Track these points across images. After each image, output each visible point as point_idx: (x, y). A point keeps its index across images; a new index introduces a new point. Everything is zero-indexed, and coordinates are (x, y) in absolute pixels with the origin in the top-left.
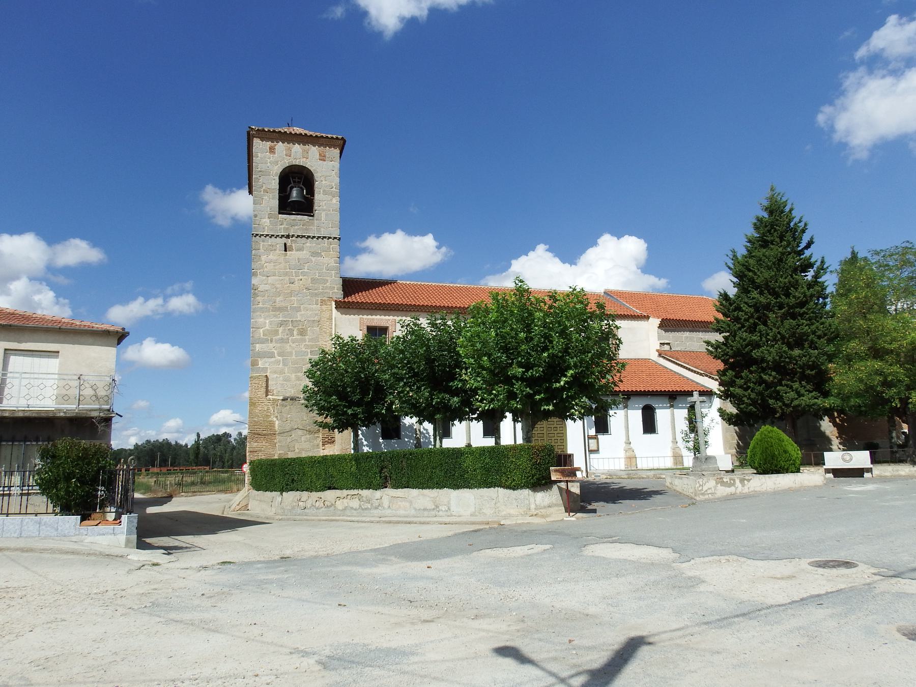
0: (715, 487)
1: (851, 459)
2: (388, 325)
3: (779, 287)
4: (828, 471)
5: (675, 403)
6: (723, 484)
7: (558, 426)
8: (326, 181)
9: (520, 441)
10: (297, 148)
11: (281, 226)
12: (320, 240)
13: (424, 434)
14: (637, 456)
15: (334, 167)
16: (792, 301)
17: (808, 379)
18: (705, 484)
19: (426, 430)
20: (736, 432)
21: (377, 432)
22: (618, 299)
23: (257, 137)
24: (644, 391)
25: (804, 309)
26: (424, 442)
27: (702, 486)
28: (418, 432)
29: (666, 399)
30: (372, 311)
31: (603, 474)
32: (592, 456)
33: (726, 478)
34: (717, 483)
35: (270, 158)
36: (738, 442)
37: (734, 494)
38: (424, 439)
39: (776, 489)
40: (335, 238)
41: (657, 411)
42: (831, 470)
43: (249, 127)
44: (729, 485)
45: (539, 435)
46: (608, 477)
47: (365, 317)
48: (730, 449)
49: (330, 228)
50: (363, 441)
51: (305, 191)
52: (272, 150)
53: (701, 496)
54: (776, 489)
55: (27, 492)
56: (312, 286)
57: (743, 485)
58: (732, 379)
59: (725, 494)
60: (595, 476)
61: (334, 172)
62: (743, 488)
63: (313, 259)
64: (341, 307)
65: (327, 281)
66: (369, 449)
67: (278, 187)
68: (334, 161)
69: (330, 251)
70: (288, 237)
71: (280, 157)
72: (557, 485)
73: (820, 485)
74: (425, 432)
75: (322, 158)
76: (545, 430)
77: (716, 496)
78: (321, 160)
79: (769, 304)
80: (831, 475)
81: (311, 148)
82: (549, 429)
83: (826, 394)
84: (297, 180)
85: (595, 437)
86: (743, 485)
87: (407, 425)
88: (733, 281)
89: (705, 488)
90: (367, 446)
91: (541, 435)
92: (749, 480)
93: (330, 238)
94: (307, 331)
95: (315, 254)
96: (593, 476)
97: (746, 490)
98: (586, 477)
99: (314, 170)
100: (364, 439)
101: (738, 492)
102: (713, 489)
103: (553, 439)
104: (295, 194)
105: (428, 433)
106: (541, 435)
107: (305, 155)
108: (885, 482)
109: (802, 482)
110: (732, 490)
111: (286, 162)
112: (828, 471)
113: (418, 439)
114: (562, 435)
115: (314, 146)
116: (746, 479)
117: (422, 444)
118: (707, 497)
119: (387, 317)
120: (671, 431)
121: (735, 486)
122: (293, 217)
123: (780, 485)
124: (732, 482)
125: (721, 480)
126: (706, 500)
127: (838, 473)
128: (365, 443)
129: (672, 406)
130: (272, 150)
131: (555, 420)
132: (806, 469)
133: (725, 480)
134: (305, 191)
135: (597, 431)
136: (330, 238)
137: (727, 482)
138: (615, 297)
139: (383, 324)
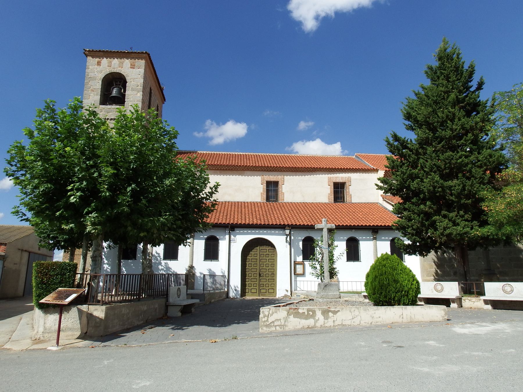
0: (286, 319)
1: (512, 291)
3: (438, 122)
4: (486, 302)
5: (378, 236)
6: (298, 315)
7: (270, 253)
8: (134, 82)
10: (116, 62)
13: (156, 257)
14: (340, 280)
15: (140, 72)
16: (448, 133)
17: (465, 208)
18: (272, 315)
19: (159, 254)
20: (434, 262)
22: (362, 159)
23: (89, 56)
24: (369, 225)
25: (462, 141)
26: (155, 263)
27: (268, 316)
28: (150, 255)
29: (370, 233)
31: (302, 294)
32: (299, 279)
33: (303, 309)
34: (289, 314)
35: (97, 69)
36: (436, 270)
37: (312, 327)
38: (155, 260)
39: (373, 323)
41: (361, 242)
42: (489, 302)
43: (84, 49)
44: (307, 317)
45: (270, 261)
46: (306, 297)
48: (428, 276)
51: (122, 90)
52: (99, 64)
53: (265, 328)
54: (373, 323)
57: (326, 318)
58: (398, 211)
59: (299, 327)
60: (297, 296)
61: (140, 76)
62: (326, 321)
66: (109, 266)
67: (100, 87)
68: (141, 69)
71: (104, 67)
72: (77, 307)
73: (438, 320)
74: (157, 255)
75: (132, 67)
76: (258, 256)
77: (287, 329)
78: (132, 68)
79: (427, 138)
80: (489, 307)
81: (125, 61)
82: (262, 256)
83: (484, 223)
84: (118, 83)
85: (302, 264)
86: (326, 318)
88: (406, 124)
89: (271, 319)
90: (107, 264)
91: (255, 260)
92: (335, 313)
96: (295, 296)
97: (330, 323)
98: (290, 296)
99: (126, 75)
100: (105, 259)
101: (318, 324)
102: (283, 322)
103: (265, 263)
104: (115, 92)
105: (160, 256)
106: (255, 260)
107: (121, 65)
108: (430, 322)
109: (413, 316)
110: (310, 322)
111: (108, 71)
112: (486, 302)
115: (128, 59)
116: (331, 311)
117: (153, 264)
118: (273, 329)
121: (314, 319)
122: (109, 107)
123: (380, 319)
124: (311, 313)
125: (296, 311)
126: (271, 333)
127: (497, 305)
128: (106, 262)
129: (375, 239)
130: (99, 64)
131: (268, 248)
132: (468, 299)
133: (301, 311)
134: (122, 90)
135: (304, 258)
137: (304, 313)
138: (361, 158)
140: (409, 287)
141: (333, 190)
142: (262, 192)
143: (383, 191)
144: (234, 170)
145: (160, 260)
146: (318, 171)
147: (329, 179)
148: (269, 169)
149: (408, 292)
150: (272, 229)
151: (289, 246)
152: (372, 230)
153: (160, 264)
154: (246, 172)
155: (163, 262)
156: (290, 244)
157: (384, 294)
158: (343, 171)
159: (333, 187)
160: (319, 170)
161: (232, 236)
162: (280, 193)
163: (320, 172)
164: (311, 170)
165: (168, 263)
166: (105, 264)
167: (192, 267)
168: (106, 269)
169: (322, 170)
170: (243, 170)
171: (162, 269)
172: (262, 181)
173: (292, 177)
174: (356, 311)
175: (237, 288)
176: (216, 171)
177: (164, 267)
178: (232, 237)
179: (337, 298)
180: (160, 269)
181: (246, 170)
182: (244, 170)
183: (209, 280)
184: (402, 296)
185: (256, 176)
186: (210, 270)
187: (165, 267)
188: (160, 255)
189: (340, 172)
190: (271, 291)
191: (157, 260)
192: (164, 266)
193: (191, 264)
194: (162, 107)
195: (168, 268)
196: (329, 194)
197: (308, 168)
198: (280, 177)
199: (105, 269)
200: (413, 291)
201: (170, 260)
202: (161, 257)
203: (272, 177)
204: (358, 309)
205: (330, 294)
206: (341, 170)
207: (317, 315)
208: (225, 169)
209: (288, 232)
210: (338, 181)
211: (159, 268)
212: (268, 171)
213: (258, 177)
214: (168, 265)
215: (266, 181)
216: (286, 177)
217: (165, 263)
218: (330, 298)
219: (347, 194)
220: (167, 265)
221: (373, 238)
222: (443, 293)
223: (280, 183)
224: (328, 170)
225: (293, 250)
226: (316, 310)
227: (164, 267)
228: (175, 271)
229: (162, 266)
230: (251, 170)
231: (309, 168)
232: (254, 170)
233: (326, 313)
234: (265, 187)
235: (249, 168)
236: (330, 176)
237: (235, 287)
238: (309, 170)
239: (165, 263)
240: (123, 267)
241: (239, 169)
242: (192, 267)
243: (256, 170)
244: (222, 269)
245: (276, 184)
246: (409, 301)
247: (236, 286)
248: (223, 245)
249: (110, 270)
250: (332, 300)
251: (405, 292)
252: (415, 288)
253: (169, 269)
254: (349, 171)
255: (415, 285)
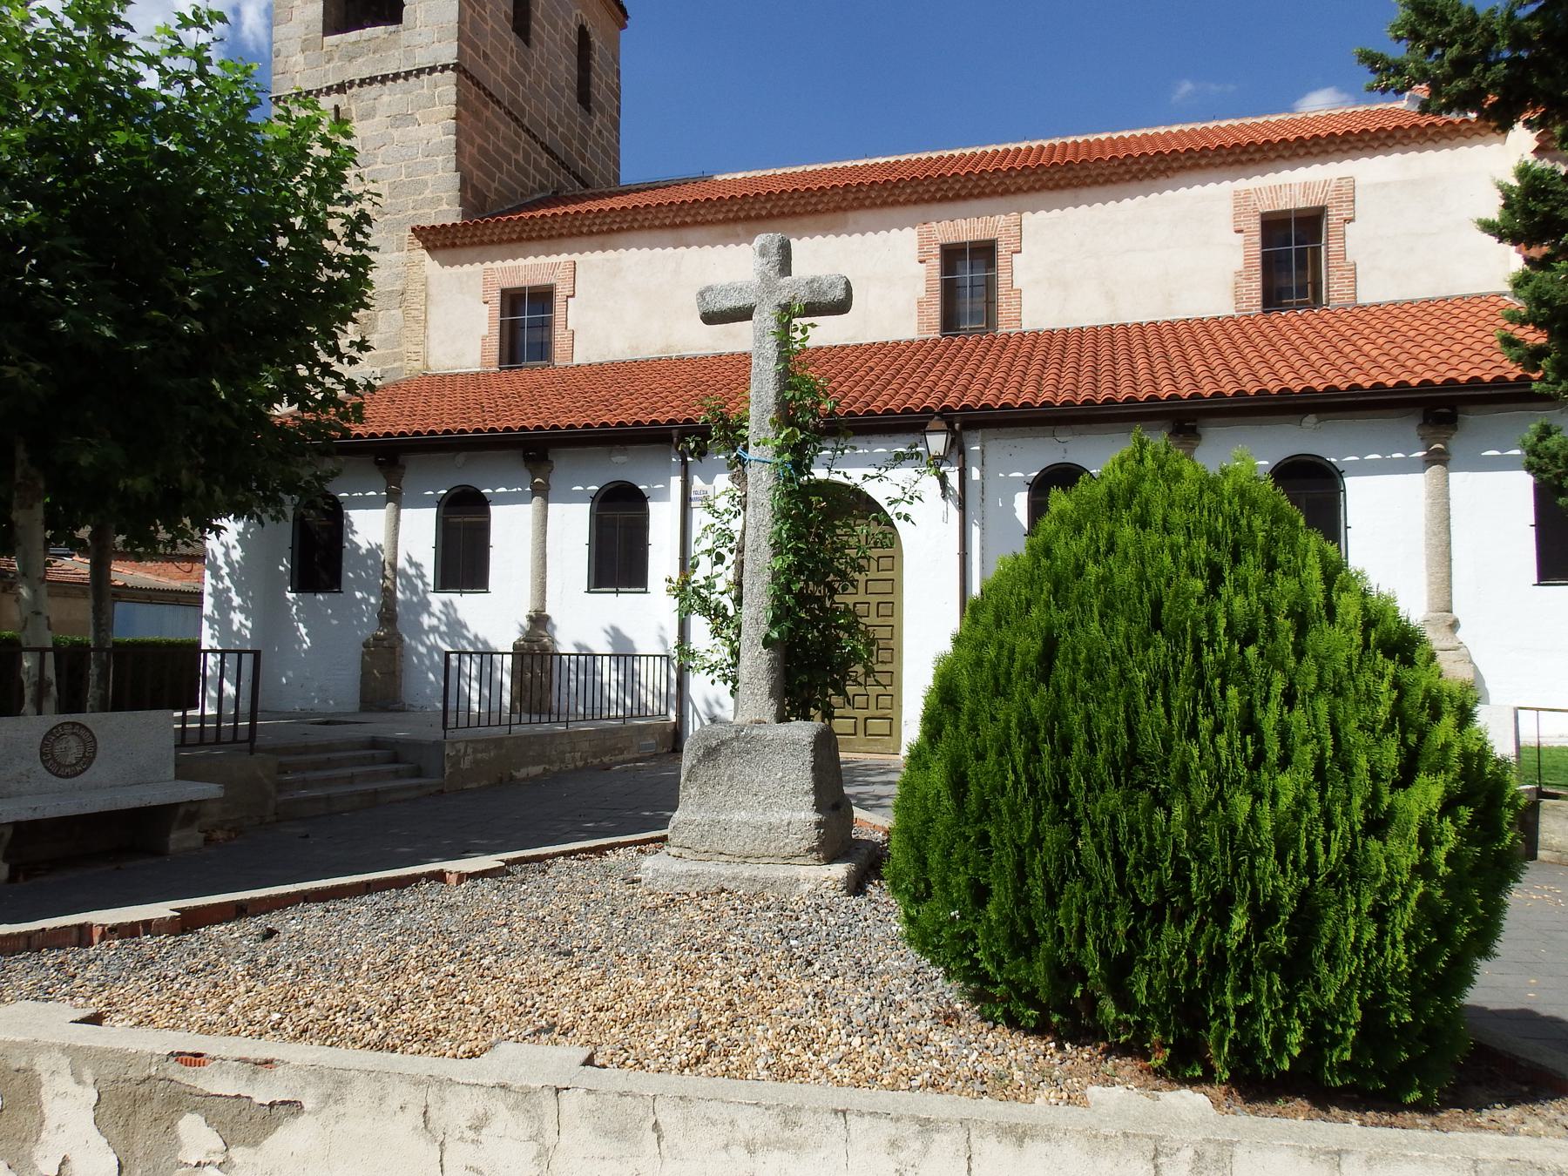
2: (553, 281)
5: (1457, 444)
9: (88, 561)
11: (327, 66)
12: (412, 80)
13: (408, 578)
19: (417, 566)
21: (281, 568)
26: (408, 604)
28: (388, 572)
29: (1410, 425)
30: (513, 246)
40: (445, 67)
41: (1351, 484)
45: (872, 587)
47: (498, 264)
49: (437, 44)
50: (233, 594)
55: (189, 713)
56: (391, 204)
63: (396, 133)
64: (436, 247)
65: (425, 184)
66: (246, 619)
69: (435, 105)
70: (341, 88)
74: (411, 571)
87: (363, 551)
90: (242, 609)
93: (432, 70)
94: (376, 320)
95: (401, 119)
105: (422, 576)
113: (388, 595)
114: (886, 587)
116: (205, 1104)
119: (554, 259)
120: (1425, 574)
128: (237, 601)
129: (1437, 458)
136: (432, 70)
139: (540, 280)
140: (1327, 861)
141: (1257, 250)
142: (924, 294)
143: (1422, 91)
144: (801, 214)
145: (425, 592)
146: (1182, 168)
147: (1241, 200)
148: (951, 188)
149: (1306, 920)
150: (875, 438)
151: (955, 514)
152: (1420, 411)
153: (425, 606)
154: (852, 216)
155: (436, 600)
156: (962, 507)
157: (1008, 920)
158: (1314, 150)
159: (1257, 239)
160: (1189, 163)
161: (696, 478)
162: (1002, 291)
163: (1196, 175)
164: (1148, 167)
165: (456, 604)
166: (234, 609)
167: (539, 620)
168: (239, 630)
169: (1203, 162)
170: (838, 209)
171: (434, 629)
172: (921, 246)
173: (1056, 212)
174: (496, 1126)
175: (717, 711)
176: (730, 229)
177: (439, 619)
178: (697, 483)
179: (789, 859)
180: (426, 627)
181: (851, 208)
182: (845, 210)
183: (609, 674)
184: (1218, 962)
185: (894, 231)
186: (616, 635)
187: (443, 617)
188: (425, 571)
189: (1297, 160)
190: (876, 726)
191: (414, 589)
192: (438, 613)
193: (537, 606)
194: (614, 45)
195: (455, 627)
196: (1238, 274)
197: (1129, 161)
198: (1001, 220)
199: (235, 628)
200: (1380, 914)
201: (461, 593)
202: (426, 580)
203: (966, 226)
204: (533, 1114)
205: (742, 816)
206: (1302, 151)
207: (50, 1124)
208: (764, 213)
209: (937, 443)
210: (1283, 204)
211: (421, 624)
212: (944, 199)
213: (908, 230)
214: (455, 610)
215: (942, 246)
216: (1027, 217)
217: (444, 604)
218: (733, 847)
219: (1333, 263)
220: (452, 611)
221: (1430, 453)
222: (98, 772)
223: (1002, 250)
224: (1230, 159)
225: (975, 532)
226: (42, 1064)
227: (439, 619)
228: (480, 636)
229: (431, 614)
230: (873, 205)
231: (1136, 161)
232: (885, 204)
233: (145, 1112)
234: (936, 274)
235: (861, 195)
236: (1242, 184)
237: (709, 705)
238: (1135, 168)
239: (444, 604)
240: (299, 621)
241: (820, 207)
242: (539, 620)
243: (895, 203)
244: (662, 628)
245: (985, 252)
246: (1318, 1041)
247: (712, 699)
248: (662, 519)
249: (251, 631)
250: (727, 871)
251: (1263, 916)
252: (1424, 870)
253: (457, 627)
254: (1345, 147)
255: (1427, 839)
